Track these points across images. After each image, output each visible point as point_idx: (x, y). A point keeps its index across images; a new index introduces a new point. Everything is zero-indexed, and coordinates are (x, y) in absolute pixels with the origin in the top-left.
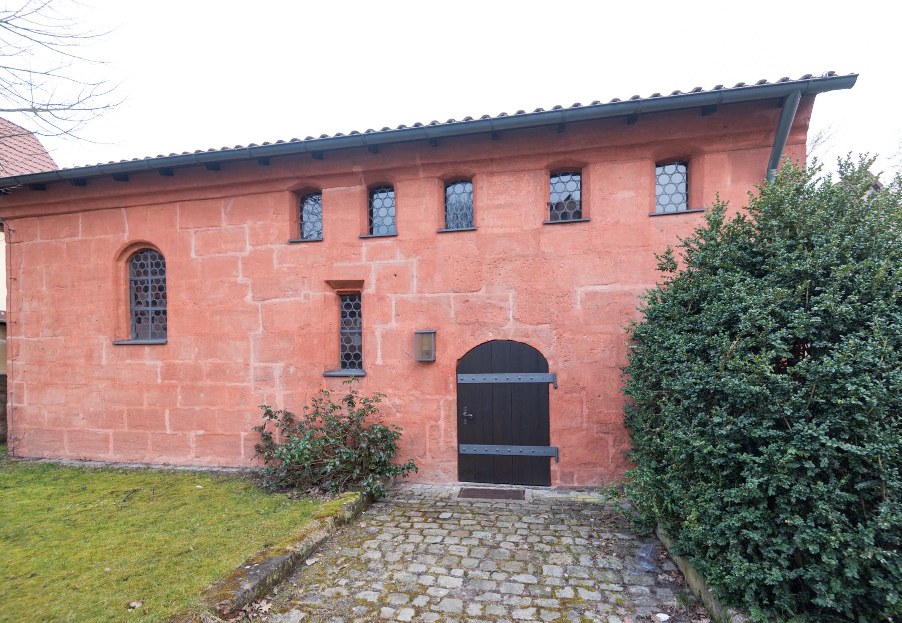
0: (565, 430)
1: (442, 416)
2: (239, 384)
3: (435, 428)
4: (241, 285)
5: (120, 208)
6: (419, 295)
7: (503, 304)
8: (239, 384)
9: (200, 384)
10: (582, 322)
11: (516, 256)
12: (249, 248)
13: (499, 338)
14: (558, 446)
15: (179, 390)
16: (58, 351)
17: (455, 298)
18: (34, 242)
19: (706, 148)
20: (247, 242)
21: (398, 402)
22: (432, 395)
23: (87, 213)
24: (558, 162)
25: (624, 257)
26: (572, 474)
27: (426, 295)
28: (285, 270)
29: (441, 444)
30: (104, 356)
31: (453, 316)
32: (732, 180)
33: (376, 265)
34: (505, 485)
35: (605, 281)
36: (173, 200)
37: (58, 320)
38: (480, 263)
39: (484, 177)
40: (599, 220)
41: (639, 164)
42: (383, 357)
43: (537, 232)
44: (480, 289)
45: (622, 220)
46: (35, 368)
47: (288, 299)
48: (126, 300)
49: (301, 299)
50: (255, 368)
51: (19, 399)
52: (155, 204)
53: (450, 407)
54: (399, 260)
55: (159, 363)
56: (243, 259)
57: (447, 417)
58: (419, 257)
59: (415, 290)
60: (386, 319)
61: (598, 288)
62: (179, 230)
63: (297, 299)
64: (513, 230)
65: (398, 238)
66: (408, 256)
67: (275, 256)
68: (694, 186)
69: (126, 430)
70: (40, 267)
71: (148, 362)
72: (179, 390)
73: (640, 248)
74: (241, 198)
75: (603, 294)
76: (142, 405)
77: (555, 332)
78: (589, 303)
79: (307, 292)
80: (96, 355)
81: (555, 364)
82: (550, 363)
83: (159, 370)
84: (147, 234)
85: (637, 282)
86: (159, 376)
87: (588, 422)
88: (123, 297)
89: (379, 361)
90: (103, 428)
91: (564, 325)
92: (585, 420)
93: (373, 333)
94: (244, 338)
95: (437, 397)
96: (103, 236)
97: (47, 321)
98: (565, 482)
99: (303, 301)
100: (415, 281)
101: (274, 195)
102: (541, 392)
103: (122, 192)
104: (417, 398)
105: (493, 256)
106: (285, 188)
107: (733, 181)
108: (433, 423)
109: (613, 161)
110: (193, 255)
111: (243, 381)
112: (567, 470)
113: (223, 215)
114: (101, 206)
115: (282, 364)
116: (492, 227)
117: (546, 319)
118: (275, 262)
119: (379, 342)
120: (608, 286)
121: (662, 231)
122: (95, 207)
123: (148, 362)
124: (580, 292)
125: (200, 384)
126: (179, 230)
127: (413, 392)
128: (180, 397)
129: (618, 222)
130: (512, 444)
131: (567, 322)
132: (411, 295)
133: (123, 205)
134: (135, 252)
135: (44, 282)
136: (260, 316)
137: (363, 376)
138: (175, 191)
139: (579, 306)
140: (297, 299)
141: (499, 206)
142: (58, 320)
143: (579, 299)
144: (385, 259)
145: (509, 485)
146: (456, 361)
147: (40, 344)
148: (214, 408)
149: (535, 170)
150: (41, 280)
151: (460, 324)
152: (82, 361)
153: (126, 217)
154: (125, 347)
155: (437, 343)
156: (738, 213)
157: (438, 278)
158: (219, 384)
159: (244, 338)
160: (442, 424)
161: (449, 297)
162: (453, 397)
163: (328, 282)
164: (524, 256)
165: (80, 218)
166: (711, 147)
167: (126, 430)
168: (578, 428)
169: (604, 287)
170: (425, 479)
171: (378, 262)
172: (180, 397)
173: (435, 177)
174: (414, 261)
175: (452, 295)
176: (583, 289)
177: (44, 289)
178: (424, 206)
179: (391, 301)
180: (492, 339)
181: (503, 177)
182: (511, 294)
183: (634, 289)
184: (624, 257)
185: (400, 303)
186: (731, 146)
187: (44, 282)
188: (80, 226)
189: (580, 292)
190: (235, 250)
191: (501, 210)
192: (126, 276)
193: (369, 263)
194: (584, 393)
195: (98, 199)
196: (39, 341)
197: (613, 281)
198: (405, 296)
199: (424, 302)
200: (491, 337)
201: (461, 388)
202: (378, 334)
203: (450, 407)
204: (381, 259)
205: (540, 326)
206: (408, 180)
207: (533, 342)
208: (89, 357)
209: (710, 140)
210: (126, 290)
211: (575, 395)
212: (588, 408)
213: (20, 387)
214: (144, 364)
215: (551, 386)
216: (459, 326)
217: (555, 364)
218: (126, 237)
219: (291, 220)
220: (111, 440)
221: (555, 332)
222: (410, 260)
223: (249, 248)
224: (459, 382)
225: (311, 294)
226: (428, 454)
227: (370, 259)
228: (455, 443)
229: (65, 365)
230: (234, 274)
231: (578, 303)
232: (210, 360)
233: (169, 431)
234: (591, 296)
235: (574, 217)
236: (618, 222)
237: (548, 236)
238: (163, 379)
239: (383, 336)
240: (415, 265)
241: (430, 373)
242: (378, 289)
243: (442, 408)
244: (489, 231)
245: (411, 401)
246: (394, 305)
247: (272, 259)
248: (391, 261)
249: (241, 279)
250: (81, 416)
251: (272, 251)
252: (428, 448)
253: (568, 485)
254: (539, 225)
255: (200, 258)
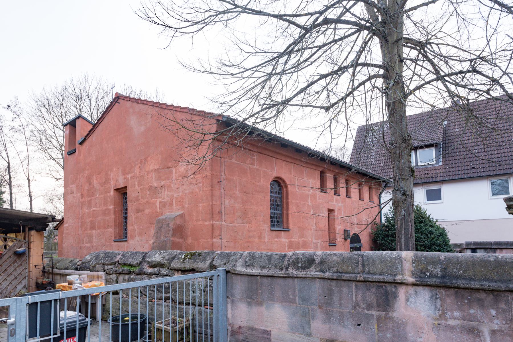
16: (245, 233)
18: (231, 161)
37: (245, 213)
46: (232, 244)
52: (286, 161)
55: (287, 241)
68: (371, 194)
70: (236, 178)
71: (284, 240)
80: (263, 236)
83: (287, 244)
84: (285, 175)
86: (287, 247)
96: (266, 170)
97: (239, 214)
103: (278, 151)
113: (305, 175)
114: (267, 154)
122: (265, 153)
123: (284, 240)
133: (276, 157)
135: (238, 188)
137: (288, 231)
138: (273, 151)
142: (245, 213)
147: (235, 228)
150: (236, 187)
152: (256, 240)
154: (275, 232)
156: (119, 103)
165: (256, 156)
177: (238, 192)
187: (238, 188)
196: (234, 226)
208: (260, 237)
214: (282, 241)
229: (248, 242)
232: (302, 239)
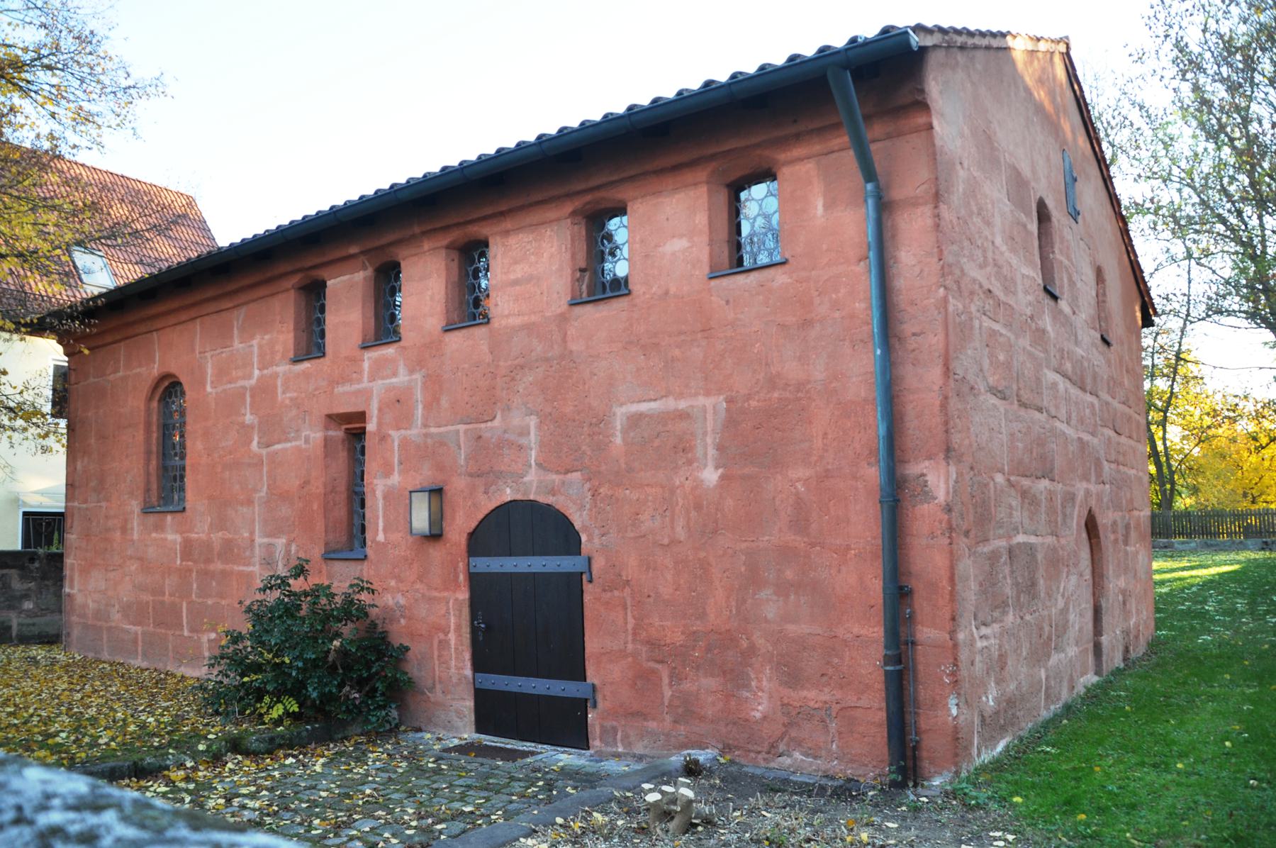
0: (604, 654)
1: (452, 627)
2: (245, 568)
3: (444, 644)
4: (248, 426)
5: (151, 331)
6: (424, 431)
7: (523, 441)
8: (245, 568)
9: (212, 567)
10: (623, 466)
11: (537, 360)
12: (256, 373)
13: (519, 497)
14: (596, 682)
15: (194, 574)
17: (466, 432)
19: (782, 157)
20: (255, 366)
21: (402, 601)
22: (440, 592)
23: (128, 341)
24: (588, 203)
25: (677, 352)
26: (615, 730)
27: (433, 430)
28: (287, 402)
29: (453, 670)
30: (136, 528)
31: (462, 462)
32: (824, 206)
33: (378, 386)
34: (528, 744)
35: (652, 394)
36: (194, 315)
38: (494, 376)
39: (498, 238)
40: (641, 292)
41: (691, 193)
42: (385, 530)
43: (563, 319)
44: (495, 417)
45: (673, 290)
47: (288, 445)
48: (158, 453)
49: (301, 443)
50: (260, 546)
51: (72, 587)
53: (460, 611)
54: (402, 378)
56: (252, 389)
57: (458, 628)
58: (424, 372)
59: (419, 422)
60: (388, 473)
61: (644, 407)
62: (198, 356)
63: (297, 443)
64: (533, 318)
65: (402, 343)
66: (411, 372)
67: (279, 383)
69: (151, 628)
72: (194, 574)
73: (699, 335)
74: (251, 305)
75: (651, 416)
76: (164, 594)
77: (587, 485)
78: (632, 434)
79: (307, 433)
81: (590, 540)
82: (584, 538)
85: (696, 395)
87: (634, 641)
88: (154, 449)
89: (381, 537)
90: (134, 625)
91: (599, 472)
92: (630, 638)
93: (374, 491)
94: (250, 502)
95: (446, 594)
98: (607, 744)
99: (304, 446)
100: (420, 407)
101: (280, 296)
102: (572, 586)
104: (423, 595)
105: (510, 363)
106: (290, 286)
107: (827, 207)
108: (441, 636)
109: (658, 193)
110: (209, 389)
111: (249, 565)
112: (608, 724)
115: (283, 541)
116: (507, 316)
117: (576, 463)
118: (280, 390)
119: (380, 506)
120: (658, 402)
121: (728, 302)
124: (621, 412)
125: (212, 567)
126: (198, 356)
127: (418, 586)
128: (195, 586)
129: (667, 293)
130: (538, 677)
131: (603, 468)
132: (414, 433)
134: (167, 388)
136: (265, 469)
139: (618, 440)
140: (297, 443)
141: (516, 282)
143: (619, 427)
144: (387, 377)
145: (533, 744)
146: (465, 535)
148: (223, 602)
149: (558, 220)
151: (471, 475)
153: (156, 342)
155: (444, 508)
157: (445, 402)
158: (228, 567)
159: (250, 502)
160: (452, 637)
161: (458, 432)
162: (464, 595)
163: (329, 416)
164: (547, 360)
166: (789, 154)
167: (151, 628)
168: (621, 651)
169: (653, 405)
170: (436, 725)
171: (380, 382)
172: (195, 586)
173: (442, 247)
174: (418, 376)
175: (462, 428)
176: (624, 409)
178: (429, 293)
179: (393, 441)
180: (509, 499)
181: (521, 235)
182: (533, 422)
183: (692, 407)
184: (677, 352)
185: (405, 443)
186: (817, 148)
188: (122, 358)
189: (621, 412)
190: (244, 378)
191: (518, 288)
192: (158, 420)
193: (371, 384)
194: (627, 590)
195: (134, 323)
197: (663, 393)
198: (409, 432)
199: (429, 441)
200: (508, 495)
201: (477, 583)
202: (379, 494)
203: (460, 611)
204: (383, 378)
205: (569, 476)
206: (412, 256)
207: (558, 502)
208: (124, 530)
209: (784, 142)
210: (158, 438)
211: (616, 593)
212: (634, 617)
213: (72, 569)
214: (166, 539)
215: (584, 577)
216: (469, 479)
217: (590, 540)
218: (155, 370)
219: (296, 329)
220: (140, 643)
221: (587, 485)
222: (414, 377)
223: (256, 373)
224: (472, 570)
225: (312, 435)
226: (438, 687)
227: (372, 379)
228: (468, 672)
230: (243, 412)
231: (618, 434)
233: (186, 633)
234: (635, 421)
235: (612, 290)
236: (667, 293)
237: (576, 324)
238: (182, 560)
239: (385, 498)
240: (420, 384)
241: (436, 553)
242: (380, 424)
243: (452, 613)
244: (504, 322)
245: (416, 600)
246: (396, 448)
247: (275, 387)
248: (394, 380)
249: (249, 418)
250: (117, 607)
251: (276, 375)
252: (437, 678)
253: (609, 749)
254: (565, 307)
255: (214, 391)
